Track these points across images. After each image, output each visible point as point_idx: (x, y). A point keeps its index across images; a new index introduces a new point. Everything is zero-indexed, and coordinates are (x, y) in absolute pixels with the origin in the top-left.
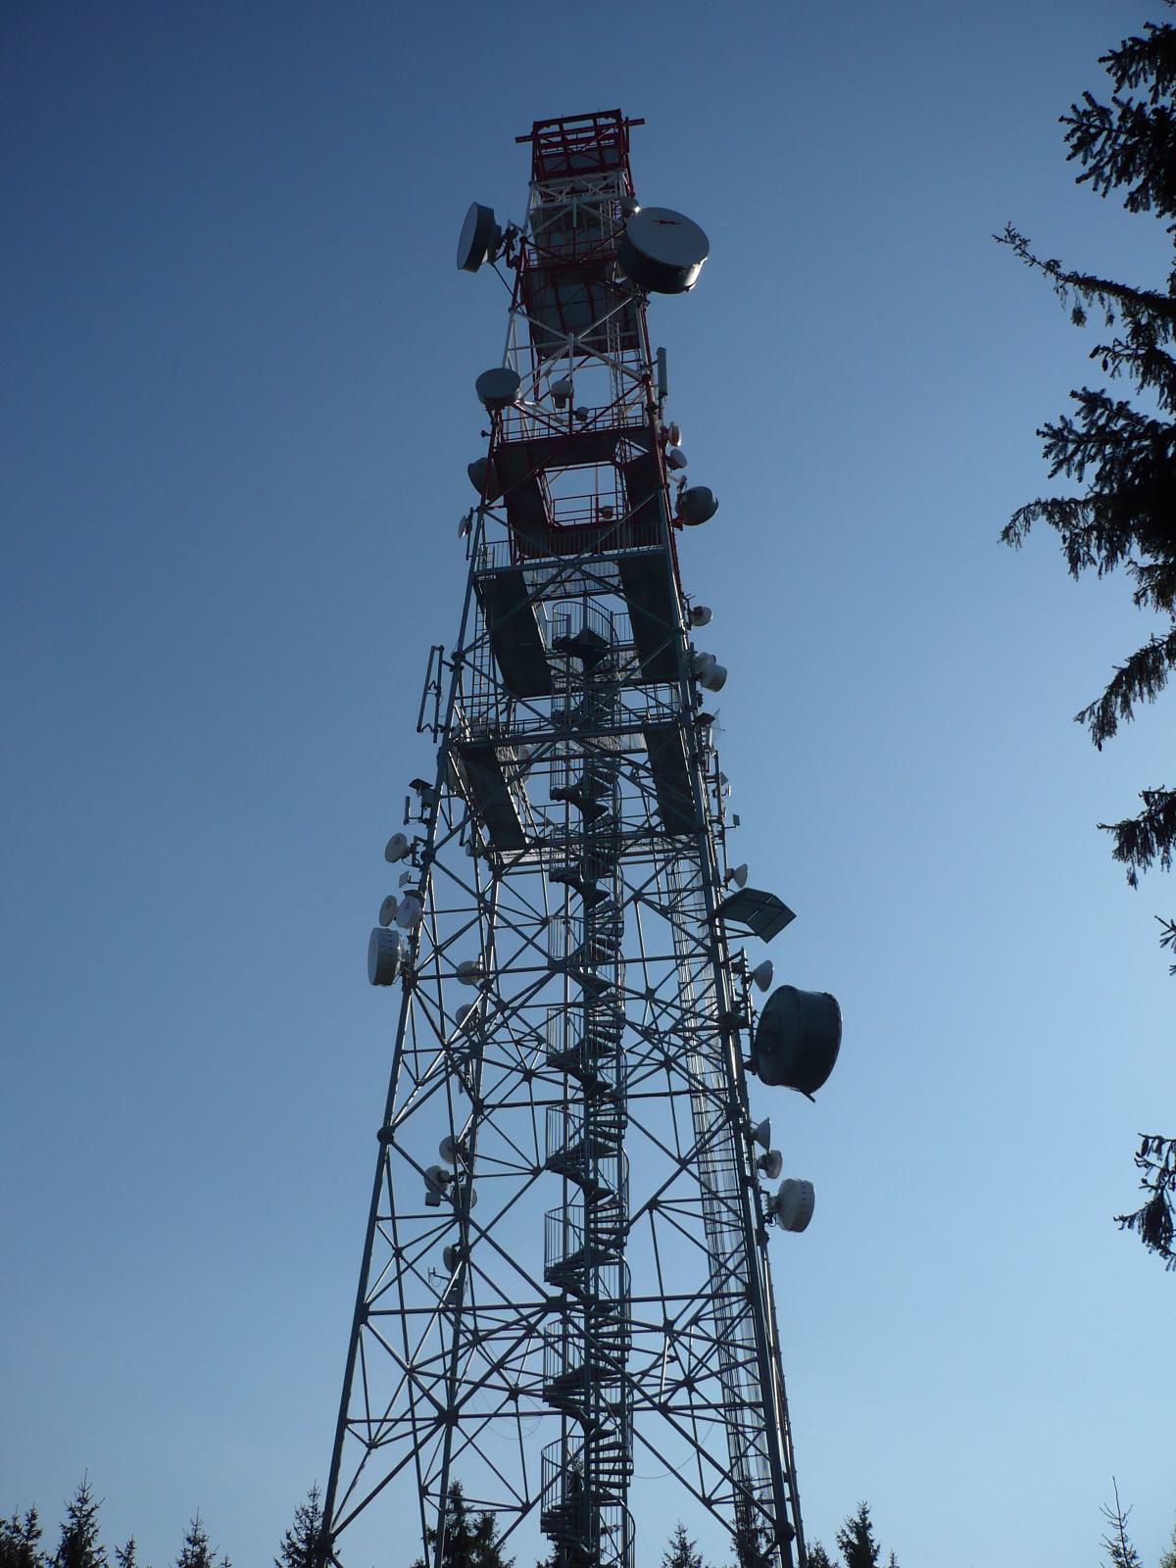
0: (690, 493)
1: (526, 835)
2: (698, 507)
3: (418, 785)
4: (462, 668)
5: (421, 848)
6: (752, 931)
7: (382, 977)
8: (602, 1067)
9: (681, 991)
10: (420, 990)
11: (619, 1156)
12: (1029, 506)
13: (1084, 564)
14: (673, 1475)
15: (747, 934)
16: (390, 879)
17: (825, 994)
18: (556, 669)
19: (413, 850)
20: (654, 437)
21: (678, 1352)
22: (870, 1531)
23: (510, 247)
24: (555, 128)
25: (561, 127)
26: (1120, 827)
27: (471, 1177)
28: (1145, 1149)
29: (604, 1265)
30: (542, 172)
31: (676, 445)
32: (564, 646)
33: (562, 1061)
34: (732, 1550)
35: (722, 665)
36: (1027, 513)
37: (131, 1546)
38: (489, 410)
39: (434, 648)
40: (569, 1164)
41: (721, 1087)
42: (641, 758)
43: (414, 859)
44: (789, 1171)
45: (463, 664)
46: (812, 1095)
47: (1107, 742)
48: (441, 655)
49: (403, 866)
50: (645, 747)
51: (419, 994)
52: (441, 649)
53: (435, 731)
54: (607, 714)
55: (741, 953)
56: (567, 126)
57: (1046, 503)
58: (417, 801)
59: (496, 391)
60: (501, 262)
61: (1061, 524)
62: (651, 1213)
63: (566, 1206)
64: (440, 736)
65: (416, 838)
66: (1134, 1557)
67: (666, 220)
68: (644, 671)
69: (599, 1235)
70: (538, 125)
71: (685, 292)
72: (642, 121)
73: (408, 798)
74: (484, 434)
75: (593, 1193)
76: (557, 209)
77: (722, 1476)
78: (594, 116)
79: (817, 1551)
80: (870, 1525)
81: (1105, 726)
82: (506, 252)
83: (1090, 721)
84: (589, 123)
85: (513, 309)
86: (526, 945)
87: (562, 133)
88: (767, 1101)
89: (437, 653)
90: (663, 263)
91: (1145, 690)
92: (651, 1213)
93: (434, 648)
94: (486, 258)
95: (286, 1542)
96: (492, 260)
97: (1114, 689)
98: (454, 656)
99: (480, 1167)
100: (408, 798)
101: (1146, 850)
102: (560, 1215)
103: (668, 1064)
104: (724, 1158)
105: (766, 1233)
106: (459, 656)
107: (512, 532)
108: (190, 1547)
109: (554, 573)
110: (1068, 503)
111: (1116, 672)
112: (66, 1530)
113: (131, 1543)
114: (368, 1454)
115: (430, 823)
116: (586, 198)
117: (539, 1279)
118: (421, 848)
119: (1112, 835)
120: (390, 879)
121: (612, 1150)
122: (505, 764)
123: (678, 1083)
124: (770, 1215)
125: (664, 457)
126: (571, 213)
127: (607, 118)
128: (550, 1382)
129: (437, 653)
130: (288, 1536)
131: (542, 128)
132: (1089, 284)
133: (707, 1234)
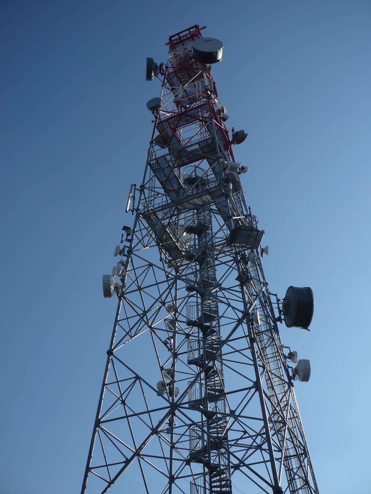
0: (237, 133)
1: (182, 251)
3: (125, 228)
5: (127, 249)
7: (107, 294)
10: (127, 299)
19: (123, 251)
21: (245, 429)
24: (177, 37)
29: (219, 400)
39: (132, 185)
44: (300, 357)
48: (135, 187)
49: (120, 258)
51: (127, 301)
52: (135, 185)
53: (133, 211)
59: (154, 106)
64: (135, 213)
70: (171, 37)
71: (218, 62)
72: (205, 27)
73: (123, 235)
74: (153, 121)
77: (148, 413)
78: (189, 29)
89: (134, 187)
90: (206, 52)
93: (132, 185)
94: (153, 74)
96: (156, 75)
98: (141, 187)
100: (123, 235)
104: (272, 357)
105: (292, 383)
115: (130, 241)
124: (294, 376)
125: (220, 118)
133: (268, 388)
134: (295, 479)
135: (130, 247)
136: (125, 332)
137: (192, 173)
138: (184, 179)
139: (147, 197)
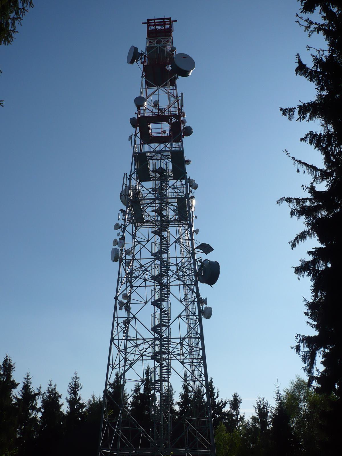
2: (188, 132)
3: (122, 210)
4: (131, 179)
5: (123, 227)
6: (203, 252)
8: (163, 279)
9: (181, 260)
11: (168, 301)
12: (283, 198)
13: (293, 215)
14: (177, 374)
15: (202, 253)
16: (115, 235)
17: (216, 262)
18: (152, 176)
20: (179, 116)
22: (213, 383)
23: (142, 58)
24: (153, 21)
25: (155, 21)
26: (296, 268)
27: (130, 304)
28: (297, 336)
30: (150, 34)
31: (184, 117)
32: (154, 171)
33: (154, 278)
34: (182, 388)
35: (197, 183)
36: (282, 199)
37: (40, 387)
38: (137, 107)
39: (124, 174)
40: (157, 303)
41: (191, 284)
42: (176, 204)
43: (121, 229)
45: (132, 178)
46: (212, 286)
47: (294, 248)
49: (119, 231)
50: (177, 202)
54: (165, 189)
55: (201, 258)
56: (156, 21)
57: (286, 198)
58: (121, 214)
59: (139, 102)
60: (139, 62)
61: (289, 202)
62: (179, 318)
63: (155, 313)
65: (122, 224)
66: (281, 394)
67: (185, 57)
68: (174, 176)
69: (163, 320)
70: (148, 20)
73: (119, 214)
74: (135, 113)
75: (162, 312)
76: (153, 47)
78: (164, 19)
79: (264, 406)
80: (213, 382)
81: (294, 245)
82: (141, 59)
83: (291, 244)
84: (163, 20)
85: (142, 77)
86: (143, 247)
87: (155, 22)
88: (204, 289)
89: (125, 175)
91: (302, 240)
92: (179, 318)
93: (124, 174)
95: (70, 385)
96: (137, 61)
97: (296, 238)
98: (129, 176)
99: (132, 301)
100: (119, 214)
101: (301, 272)
102: (153, 315)
103: (179, 279)
106: (131, 176)
107: (141, 140)
108: (49, 386)
109: (154, 154)
110: (290, 198)
111: (297, 235)
112: (24, 383)
113: (40, 386)
114: (112, 370)
115: (125, 220)
116: (162, 44)
117: (150, 331)
118: (123, 227)
119: (294, 269)
120: (115, 235)
121: (166, 300)
122: (142, 204)
123: (181, 283)
126: (158, 47)
127: (167, 20)
128: (152, 354)
129: (125, 175)
130: (70, 384)
131: (150, 21)
132: (300, 162)
134: (195, 371)
135: (124, 225)
136: (120, 339)
137: (159, 146)
138: (151, 328)
139: (128, 352)
